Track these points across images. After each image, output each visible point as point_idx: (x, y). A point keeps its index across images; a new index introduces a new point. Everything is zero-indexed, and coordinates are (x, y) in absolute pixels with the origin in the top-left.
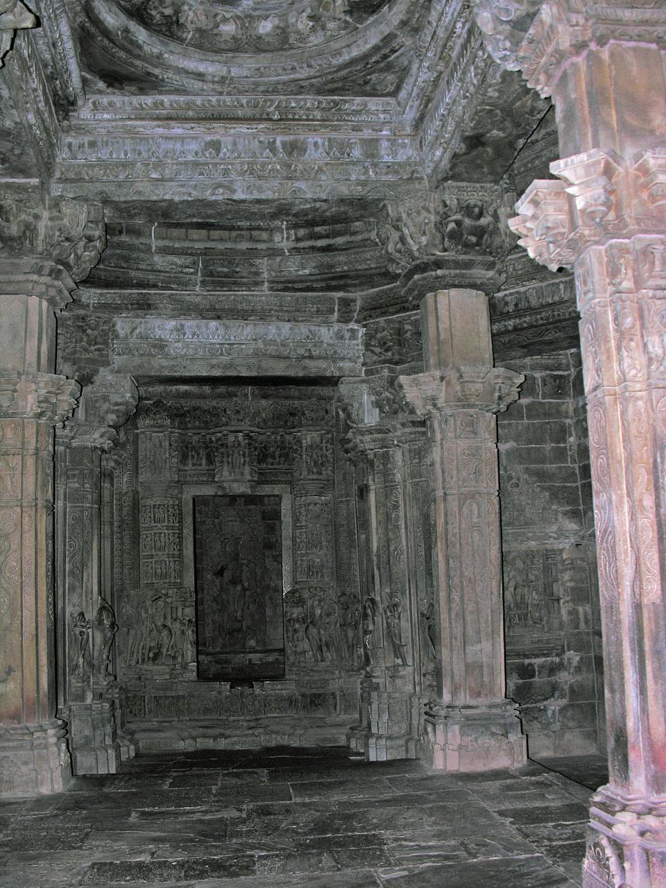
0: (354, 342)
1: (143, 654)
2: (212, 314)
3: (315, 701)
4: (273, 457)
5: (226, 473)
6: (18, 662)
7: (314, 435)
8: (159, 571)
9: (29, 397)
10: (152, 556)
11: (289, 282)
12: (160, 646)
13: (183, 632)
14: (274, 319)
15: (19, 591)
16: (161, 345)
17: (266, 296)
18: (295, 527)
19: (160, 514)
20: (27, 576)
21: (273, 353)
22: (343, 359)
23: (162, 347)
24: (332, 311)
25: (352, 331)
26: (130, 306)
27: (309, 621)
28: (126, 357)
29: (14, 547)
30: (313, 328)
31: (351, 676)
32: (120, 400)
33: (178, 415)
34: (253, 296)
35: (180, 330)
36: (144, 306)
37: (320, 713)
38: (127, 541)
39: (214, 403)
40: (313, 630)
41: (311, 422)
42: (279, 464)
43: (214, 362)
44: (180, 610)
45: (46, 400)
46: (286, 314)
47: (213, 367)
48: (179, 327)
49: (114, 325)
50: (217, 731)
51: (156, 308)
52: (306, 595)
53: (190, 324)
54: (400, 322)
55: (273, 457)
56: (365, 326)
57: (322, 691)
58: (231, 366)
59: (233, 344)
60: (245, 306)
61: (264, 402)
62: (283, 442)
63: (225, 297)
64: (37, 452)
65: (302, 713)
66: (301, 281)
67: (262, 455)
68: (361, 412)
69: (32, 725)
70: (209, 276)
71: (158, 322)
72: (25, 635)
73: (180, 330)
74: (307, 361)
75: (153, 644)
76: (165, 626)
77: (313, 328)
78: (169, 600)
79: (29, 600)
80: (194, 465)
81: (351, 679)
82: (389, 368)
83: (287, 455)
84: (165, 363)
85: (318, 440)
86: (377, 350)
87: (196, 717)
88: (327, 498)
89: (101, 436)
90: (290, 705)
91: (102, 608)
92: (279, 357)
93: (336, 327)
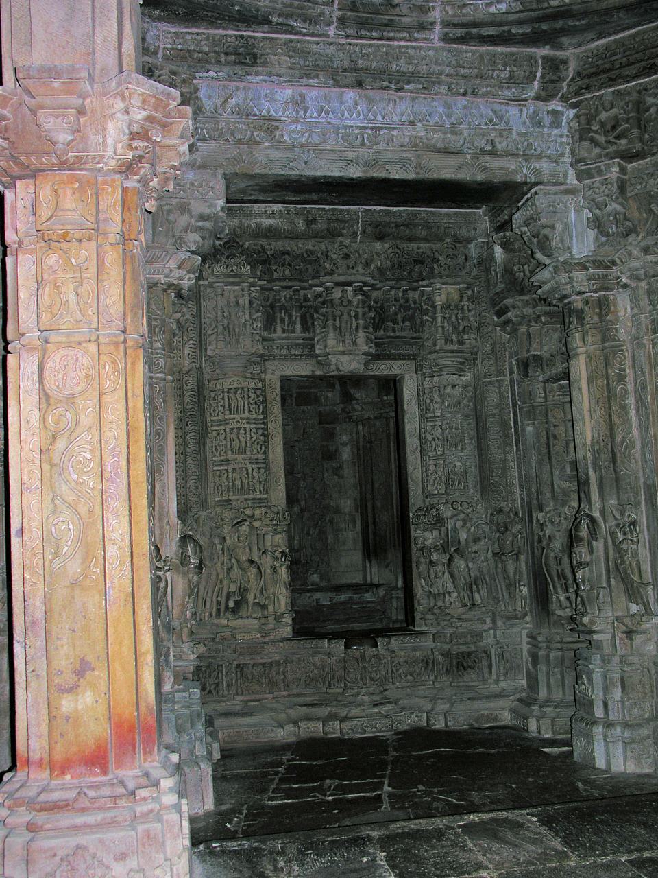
0: (556, 131)
1: (219, 603)
2: (351, 78)
3: (462, 662)
4: (395, 321)
5: (331, 342)
6: (100, 648)
7: (451, 289)
8: (238, 483)
9: (111, 127)
10: (227, 462)
11: (475, 24)
12: (243, 592)
13: (275, 571)
14: (443, 89)
15: (98, 508)
16: (269, 126)
17: (436, 50)
18: (423, 418)
19: (238, 401)
20: (111, 480)
21: (439, 145)
22: (539, 157)
23: (271, 130)
24: (531, 77)
25: (554, 113)
26: (223, 58)
27: (452, 549)
28: (213, 143)
29: (85, 421)
30: (497, 107)
31: (512, 626)
32: (207, 211)
33: (261, 261)
34: (414, 48)
35: (299, 102)
36: (246, 58)
37: (470, 679)
38: (191, 441)
39: (309, 245)
40: (460, 564)
41: (446, 272)
42: (403, 330)
43: (351, 155)
44: (268, 538)
45: (143, 135)
46: (462, 82)
47: (349, 162)
48: (297, 97)
49: (196, 90)
50: (323, 711)
51: (265, 63)
52: (447, 512)
53: (315, 93)
54: (639, 92)
55: (395, 321)
56: (574, 106)
57: (473, 648)
58: (374, 163)
59: (379, 129)
60: (403, 65)
61: (378, 245)
62: (407, 301)
63: (374, 49)
64: (124, 238)
65: (446, 680)
66: (492, 24)
67: (379, 318)
68: (566, 237)
69: (129, 774)
70: (351, 10)
71: (265, 90)
72: (112, 594)
73: (299, 102)
74: (487, 158)
75: (233, 589)
76: (251, 562)
77: (497, 107)
78: (256, 524)
79: (117, 527)
80: (284, 331)
81: (514, 630)
82: (620, 164)
83: (412, 319)
84: (275, 155)
85: (456, 297)
86: (601, 139)
87: (296, 692)
88: (467, 378)
89: (179, 267)
90: (426, 668)
91: (185, 538)
92: (446, 151)
93: (531, 106)
